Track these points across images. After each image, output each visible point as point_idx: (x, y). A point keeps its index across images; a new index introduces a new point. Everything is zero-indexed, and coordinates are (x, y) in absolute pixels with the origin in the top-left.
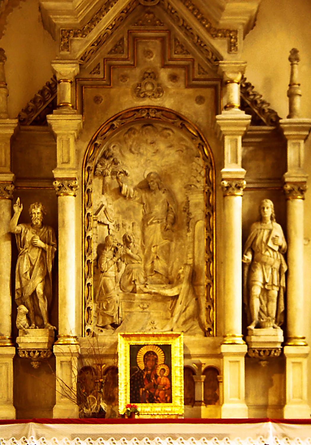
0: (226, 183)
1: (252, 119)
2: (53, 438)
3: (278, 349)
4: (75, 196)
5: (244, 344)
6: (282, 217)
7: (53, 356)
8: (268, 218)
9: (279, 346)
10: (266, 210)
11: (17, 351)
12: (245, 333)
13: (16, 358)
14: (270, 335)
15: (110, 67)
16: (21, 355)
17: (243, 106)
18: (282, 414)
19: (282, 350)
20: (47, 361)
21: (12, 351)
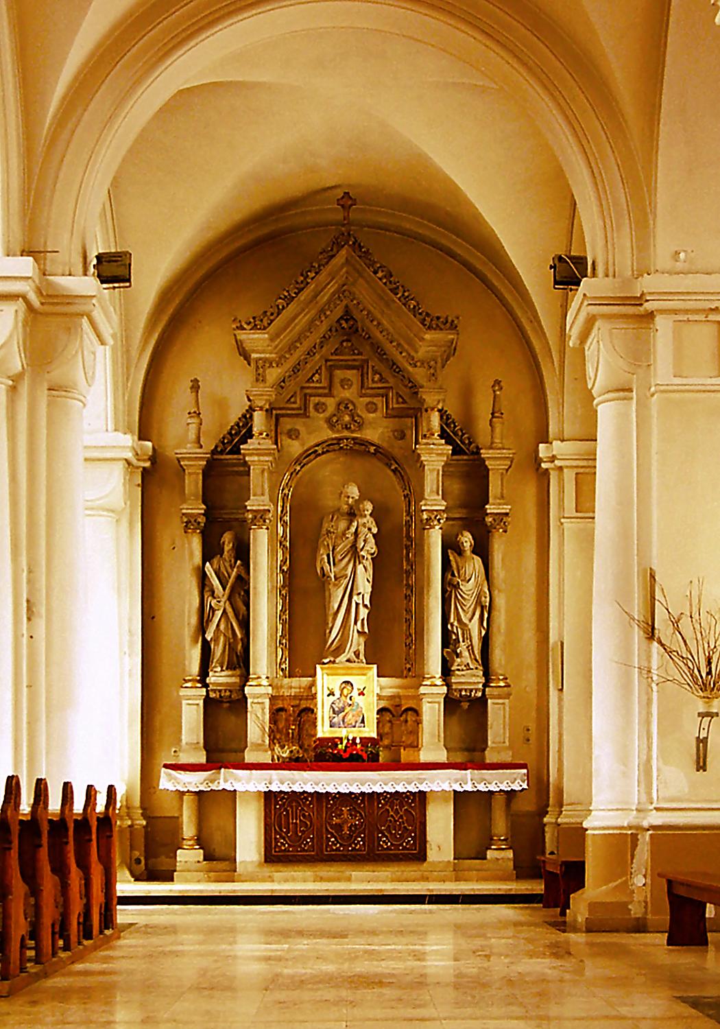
0: (425, 516)
4: (267, 529)
5: (442, 685)
6: (482, 550)
8: (468, 553)
9: (480, 686)
11: (207, 692)
12: (446, 672)
13: (208, 701)
14: (469, 679)
15: (305, 395)
16: (212, 695)
18: (484, 758)
20: (238, 703)
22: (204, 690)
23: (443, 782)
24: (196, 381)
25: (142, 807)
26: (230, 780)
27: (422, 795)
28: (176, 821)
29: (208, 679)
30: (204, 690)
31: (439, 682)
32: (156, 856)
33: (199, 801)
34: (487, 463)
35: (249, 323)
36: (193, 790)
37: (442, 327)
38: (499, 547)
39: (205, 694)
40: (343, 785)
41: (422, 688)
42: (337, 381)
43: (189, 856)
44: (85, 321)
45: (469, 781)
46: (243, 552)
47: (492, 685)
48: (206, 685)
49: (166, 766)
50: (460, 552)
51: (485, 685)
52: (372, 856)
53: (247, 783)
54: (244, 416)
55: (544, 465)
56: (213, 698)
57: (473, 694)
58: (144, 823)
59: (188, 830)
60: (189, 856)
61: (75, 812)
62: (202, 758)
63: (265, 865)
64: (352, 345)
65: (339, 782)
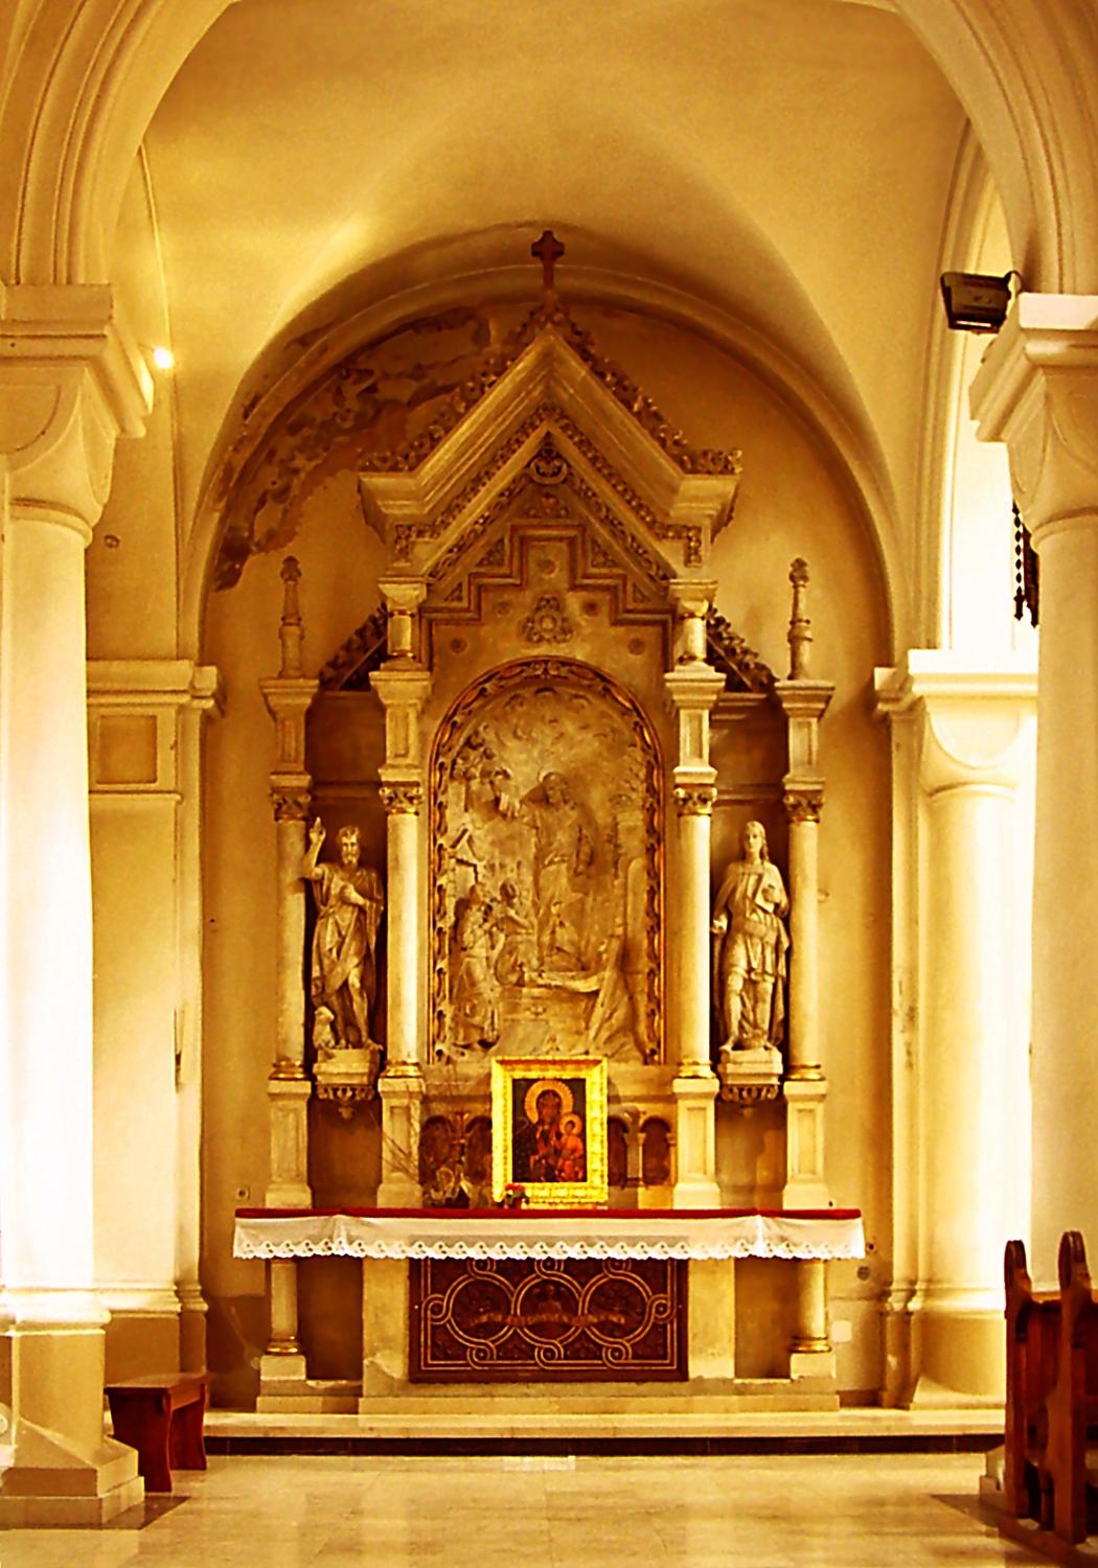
1: (728, 681)
2: (805, 1244)
3: (773, 1086)
4: (417, 813)
6: (781, 854)
7: (377, 1098)
10: (752, 840)
11: (314, 1088)
14: (758, 1062)
15: (480, 588)
17: (711, 658)
19: (781, 1088)
20: (367, 1106)
21: (306, 1088)
22: (309, 1084)
23: (297, 1244)
24: (291, 561)
25: (201, 1281)
26: (345, 1237)
27: (682, 1266)
28: (260, 1305)
29: (315, 1066)
30: (309, 1084)
31: (706, 1071)
32: (1045, 373)
33: (298, 1268)
34: (785, 705)
35: (384, 460)
36: (284, 1256)
37: (711, 467)
38: (807, 836)
39: (309, 1091)
40: (537, 1247)
41: (677, 1082)
42: (532, 565)
43: (281, 1368)
44: (88, 377)
45: (761, 1237)
46: (376, 861)
47: (793, 1077)
48: (310, 1076)
49: (241, 1213)
50: (743, 856)
51: (783, 1078)
52: (583, 1365)
53: (387, 1243)
54: (373, 620)
55: (881, 707)
56: (323, 1100)
57: (763, 1093)
58: (205, 1307)
59: (282, 1316)
60: (281, 1368)
61: (629, 1176)
62: (302, 1197)
63: (412, 1387)
64: (557, 503)
65: (611, 1241)
